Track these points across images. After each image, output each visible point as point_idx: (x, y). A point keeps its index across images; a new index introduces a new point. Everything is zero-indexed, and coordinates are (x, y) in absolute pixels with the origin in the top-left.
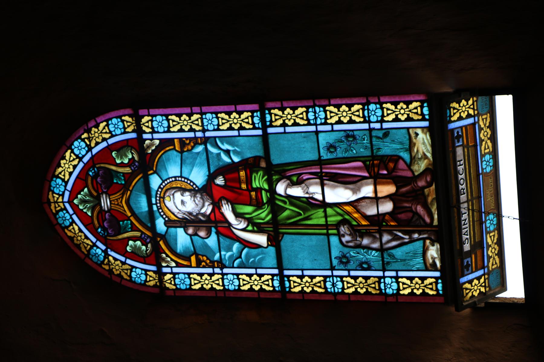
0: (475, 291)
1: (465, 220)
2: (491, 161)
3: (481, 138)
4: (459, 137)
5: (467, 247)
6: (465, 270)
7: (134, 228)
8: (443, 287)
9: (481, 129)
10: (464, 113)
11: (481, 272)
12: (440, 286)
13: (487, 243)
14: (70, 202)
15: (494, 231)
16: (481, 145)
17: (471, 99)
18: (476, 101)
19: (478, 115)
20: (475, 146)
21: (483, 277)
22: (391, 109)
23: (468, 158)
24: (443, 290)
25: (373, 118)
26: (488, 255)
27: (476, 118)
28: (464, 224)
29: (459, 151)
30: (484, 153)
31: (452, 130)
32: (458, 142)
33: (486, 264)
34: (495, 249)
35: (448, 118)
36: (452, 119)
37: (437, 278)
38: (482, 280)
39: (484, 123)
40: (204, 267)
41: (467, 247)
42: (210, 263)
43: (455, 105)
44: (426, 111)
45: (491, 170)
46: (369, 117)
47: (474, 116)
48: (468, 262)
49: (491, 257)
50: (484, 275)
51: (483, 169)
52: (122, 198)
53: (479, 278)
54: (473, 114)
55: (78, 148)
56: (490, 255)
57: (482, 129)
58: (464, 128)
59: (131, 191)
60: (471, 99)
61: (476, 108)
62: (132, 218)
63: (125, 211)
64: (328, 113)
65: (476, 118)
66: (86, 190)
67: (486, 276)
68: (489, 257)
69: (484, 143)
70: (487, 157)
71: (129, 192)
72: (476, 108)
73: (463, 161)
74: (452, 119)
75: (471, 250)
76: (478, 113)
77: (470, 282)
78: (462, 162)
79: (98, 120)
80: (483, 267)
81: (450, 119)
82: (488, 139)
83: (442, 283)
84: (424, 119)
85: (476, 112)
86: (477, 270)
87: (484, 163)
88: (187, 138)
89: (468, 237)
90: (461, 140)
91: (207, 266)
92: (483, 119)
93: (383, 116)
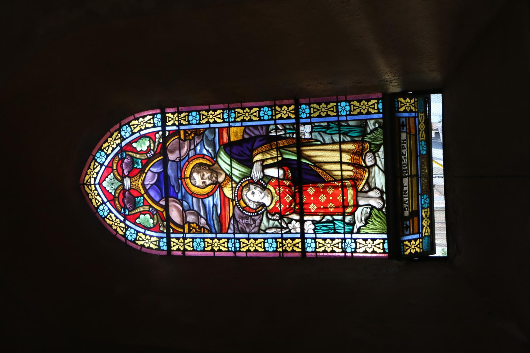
0: (412, 250)
1: (406, 191)
2: (428, 199)
3: (423, 225)
4: (403, 125)
5: (407, 213)
6: (405, 230)
7: (146, 203)
8: (388, 246)
9: (423, 219)
10: (413, 244)
11: (416, 236)
12: (386, 246)
13: (422, 216)
14: (100, 184)
15: (427, 208)
16: (419, 133)
17: (413, 99)
18: (422, 242)
19: (418, 112)
20: (416, 135)
21: (418, 240)
22: (362, 243)
23: (410, 158)
24: (388, 249)
25: (348, 250)
26: (419, 128)
27: (416, 114)
28: (405, 194)
29: (404, 136)
30: (421, 140)
31: (399, 118)
32: (403, 129)
33: (421, 231)
34: (428, 222)
35: (403, 253)
36: (400, 110)
37: (384, 239)
38: (418, 242)
39: (427, 229)
40: (194, 233)
41: (407, 213)
42: (198, 229)
43: (401, 99)
44: (380, 106)
45: (425, 154)
46: (346, 249)
47: (415, 112)
48: (407, 224)
49: (425, 226)
50: (420, 238)
51: (420, 151)
52: (139, 179)
53: (415, 240)
54: (414, 110)
55: (193, 117)
56: (424, 225)
57: (420, 123)
58: (407, 119)
59: (146, 173)
60: (413, 99)
61: (421, 248)
62: (145, 196)
63: (140, 190)
64: (317, 243)
65: (416, 114)
66: (112, 174)
67: (421, 240)
68: (423, 226)
69: (424, 228)
70: (423, 143)
71: (144, 174)
72: (421, 248)
73: (408, 201)
74: (400, 110)
75: (409, 216)
76: (418, 110)
77: (410, 241)
78: (407, 192)
79: (139, 248)
80: (419, 233)
81: (404, 253)
82: (428, 226)
83: (388, 243)
84: (379, 113)
85: (416, 110)
86: (413, 234)
87: (421, 146)
88: (189, 130)
89: (406, 156)
90: (408, 230)
91: (196, 232)
92: (425, 212)
93: (356, 248)
